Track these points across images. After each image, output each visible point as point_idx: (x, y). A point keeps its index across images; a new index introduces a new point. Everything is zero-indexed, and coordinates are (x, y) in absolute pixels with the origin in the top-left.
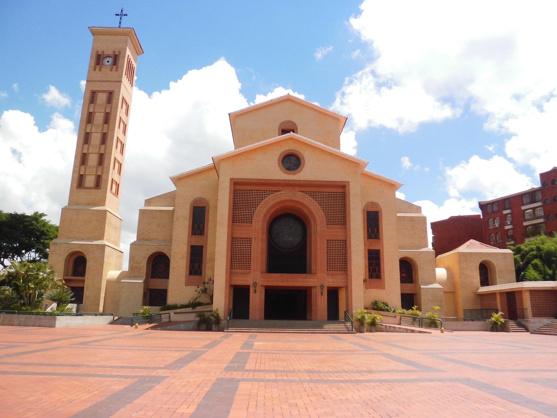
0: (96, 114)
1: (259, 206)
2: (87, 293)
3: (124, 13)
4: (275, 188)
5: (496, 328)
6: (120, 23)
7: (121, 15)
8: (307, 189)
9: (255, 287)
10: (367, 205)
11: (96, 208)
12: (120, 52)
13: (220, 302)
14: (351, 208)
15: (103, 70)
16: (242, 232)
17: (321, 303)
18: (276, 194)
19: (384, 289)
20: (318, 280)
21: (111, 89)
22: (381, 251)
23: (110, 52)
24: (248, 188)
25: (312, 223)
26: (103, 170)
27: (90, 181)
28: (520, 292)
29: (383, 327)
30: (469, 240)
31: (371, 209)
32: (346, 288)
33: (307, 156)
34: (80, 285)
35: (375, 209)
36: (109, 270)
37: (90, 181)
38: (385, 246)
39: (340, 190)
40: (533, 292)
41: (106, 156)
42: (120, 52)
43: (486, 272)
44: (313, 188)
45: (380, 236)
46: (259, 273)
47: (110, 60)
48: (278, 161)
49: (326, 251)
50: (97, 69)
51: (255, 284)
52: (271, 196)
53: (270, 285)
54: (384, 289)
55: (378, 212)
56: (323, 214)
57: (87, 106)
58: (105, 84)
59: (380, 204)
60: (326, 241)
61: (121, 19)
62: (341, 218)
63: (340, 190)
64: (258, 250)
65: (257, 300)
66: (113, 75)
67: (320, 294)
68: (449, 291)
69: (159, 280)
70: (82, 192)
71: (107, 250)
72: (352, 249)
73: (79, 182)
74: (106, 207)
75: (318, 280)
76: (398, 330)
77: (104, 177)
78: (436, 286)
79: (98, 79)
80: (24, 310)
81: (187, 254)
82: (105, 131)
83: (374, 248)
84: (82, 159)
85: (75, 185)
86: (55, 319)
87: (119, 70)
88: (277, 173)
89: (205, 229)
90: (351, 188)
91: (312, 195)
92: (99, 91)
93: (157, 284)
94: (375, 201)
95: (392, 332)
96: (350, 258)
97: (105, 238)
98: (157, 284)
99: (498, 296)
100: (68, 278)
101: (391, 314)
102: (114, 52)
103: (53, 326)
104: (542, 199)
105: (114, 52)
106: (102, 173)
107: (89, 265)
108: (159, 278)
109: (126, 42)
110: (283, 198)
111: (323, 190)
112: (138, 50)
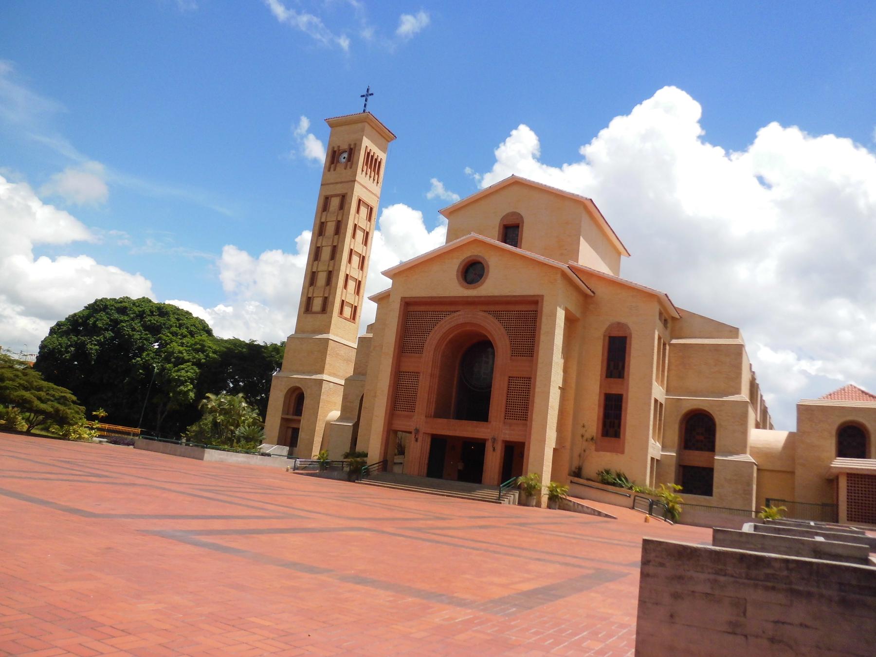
0: (329, 224)
1: (433, 331)
2: (302, 435)
3: (370, 92)
4: (452, 308)
6: (365, 105)
7: (367, 95)
8: (492, 308)
9: (494, 442)
10: (612, 326)
12: (355, 144)
13: (373, 446)
14: (542, 332)
15: (338, 169)
16: (409, 365)
17: (493, 461)
19: (623, 452)
20: (495, 431)
21: (344, 191)
22: (624, 396)
23: (345, 146)
24: (422, 308)
26: (330, 290)
27: (317, 304)
29: (571, 504)
31: (615, 333)
34: (295, 426)
35: (621, 334)
36: (331, 410)
37: (317, 304)
38: (630, 389)
39: (532, 308)
41: (335, 273)
42: (355, 144)
45: (626, 374)
46: (423, 417)
47: (346, 155)
49: (505, 391)
50: (332, 169)
51: (494, 440)
52: (447, 318)
54: (623, 452)
55: (625, 338)
56: (508, 342)
57: (319, 215)
58: (339, 186)
59: (630, 325)
60: (507, 378)
61: (366, 100)
63: (532, 308)
64: (425, 388)
65: (417, 451)
66: (349, 171)
68: (779, 469)
69: (697, 453)
70: (309, 317)
71: (325, 384)
72: (537, 390)
73: (307, 306)
74: (331, 336)
75: (495, 431)
76: (585, 509)
77: (331, 299)
78: (747, 457)
79: (332, 181)
80: (811, 527)
81: (599, 406)
82: (335, 244)
83: (614, 391)
84: (311, 278)
85: (303, 310)
86: (204, 452)
87: (354, 166)
88: (455, 289)
89: (626, 369)
90: (545, 303)
91: (497, 315)
92: (332, 196)
93: (697, 458)
94: (623, 320)
95: (580, 512)
96: (533, 402)
97: (325, 371)
98: (697, 458)
99: (843, 483)
100: (290, 417)
101: (624, 490)
102: (350, 145)
103: (202, 459)
105: (350, 145)
106: (329, 294)
107: (307, 402)
108: (697, 449)
109: (363, 130)
110: (461, 321)
111: (511, 308)
112: (385, 136)
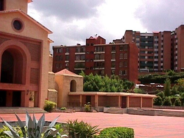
5: (87, 111)
11: (144, 85)
18: (8, 41)
25: (24, 59)
28: (94, 96)
30: (64, 69)
32: (38, 92)
33: (25, 23)
40: (100, 96)
43: (73, 84)
44: (26, 40)
48: (12, 23)
53: (4, 89)
60: (30, 68)
62: (38, 58)
67: (26, 94)
91: (25, 44)
95: (55, 112)
104: (86, 51)
111: (31, 42)
